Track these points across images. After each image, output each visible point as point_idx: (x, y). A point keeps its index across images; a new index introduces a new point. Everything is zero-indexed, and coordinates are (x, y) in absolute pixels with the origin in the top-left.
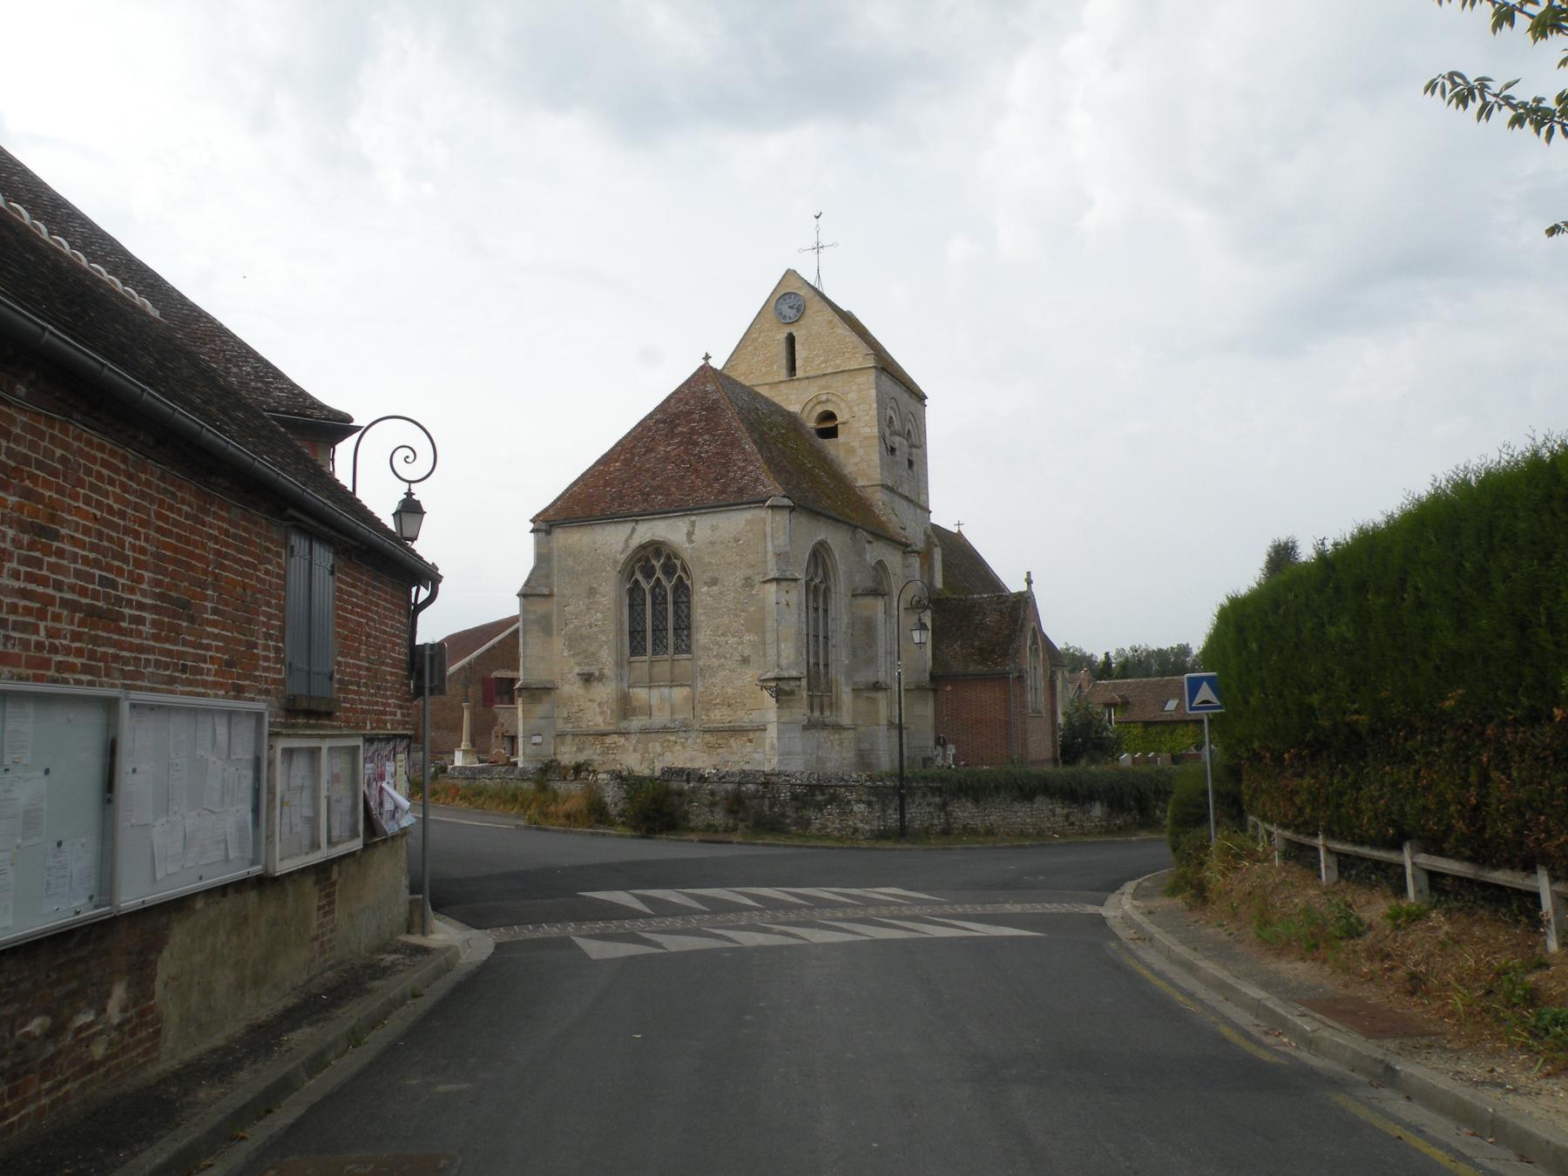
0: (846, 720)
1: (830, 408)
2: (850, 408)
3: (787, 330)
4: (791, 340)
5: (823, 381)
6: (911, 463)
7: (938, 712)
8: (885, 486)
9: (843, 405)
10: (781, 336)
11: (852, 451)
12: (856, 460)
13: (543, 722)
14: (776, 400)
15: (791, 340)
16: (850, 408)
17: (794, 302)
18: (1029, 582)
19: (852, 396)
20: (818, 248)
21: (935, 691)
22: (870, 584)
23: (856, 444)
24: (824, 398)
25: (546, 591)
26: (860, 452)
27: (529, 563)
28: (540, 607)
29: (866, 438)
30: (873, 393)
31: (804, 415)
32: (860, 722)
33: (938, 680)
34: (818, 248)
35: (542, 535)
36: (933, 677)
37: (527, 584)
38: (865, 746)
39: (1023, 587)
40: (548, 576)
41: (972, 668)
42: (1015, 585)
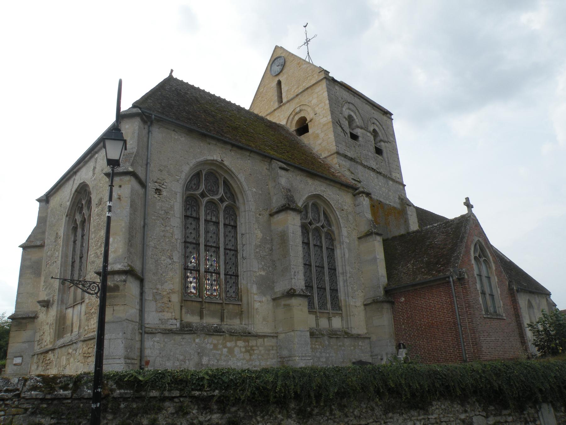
0: (260, 325)
1: (302, 115)
2: (313, 109)
3: (276, 80)
4: (279, 83)
5: (297, 100)
6: (379, 151)
7: (396, 321)
8: (338, 153)
9: (309, 109)
10: (274, 84)
11: (317, 136)
12: (319, 142)
13: (26, 345)
14: (274, 121)
15: (279, 83)
16: (313, 109)
17: (280, 61)
18: (468, 204)
19: (314, 101)
20: (307, 42)
21: (392, 303)
22: (283, 202)
23: (319, 131)
24: (298, 109)
25: (38, 243)
26: (322, 135)
27: (32, 223)
28: (35, 255)
29: (324, 125)
30: (326, 94)
31: (288, 126)
32: (280, 330)
33: (390, 295)
34: (307, 42)
35: (44, 203)
36: (388, 291)
37: (29, 240)
38: (285, 353)
39: (464, 211)
40: (44, 233)
41: (419, 278)
42: (452, 211)
